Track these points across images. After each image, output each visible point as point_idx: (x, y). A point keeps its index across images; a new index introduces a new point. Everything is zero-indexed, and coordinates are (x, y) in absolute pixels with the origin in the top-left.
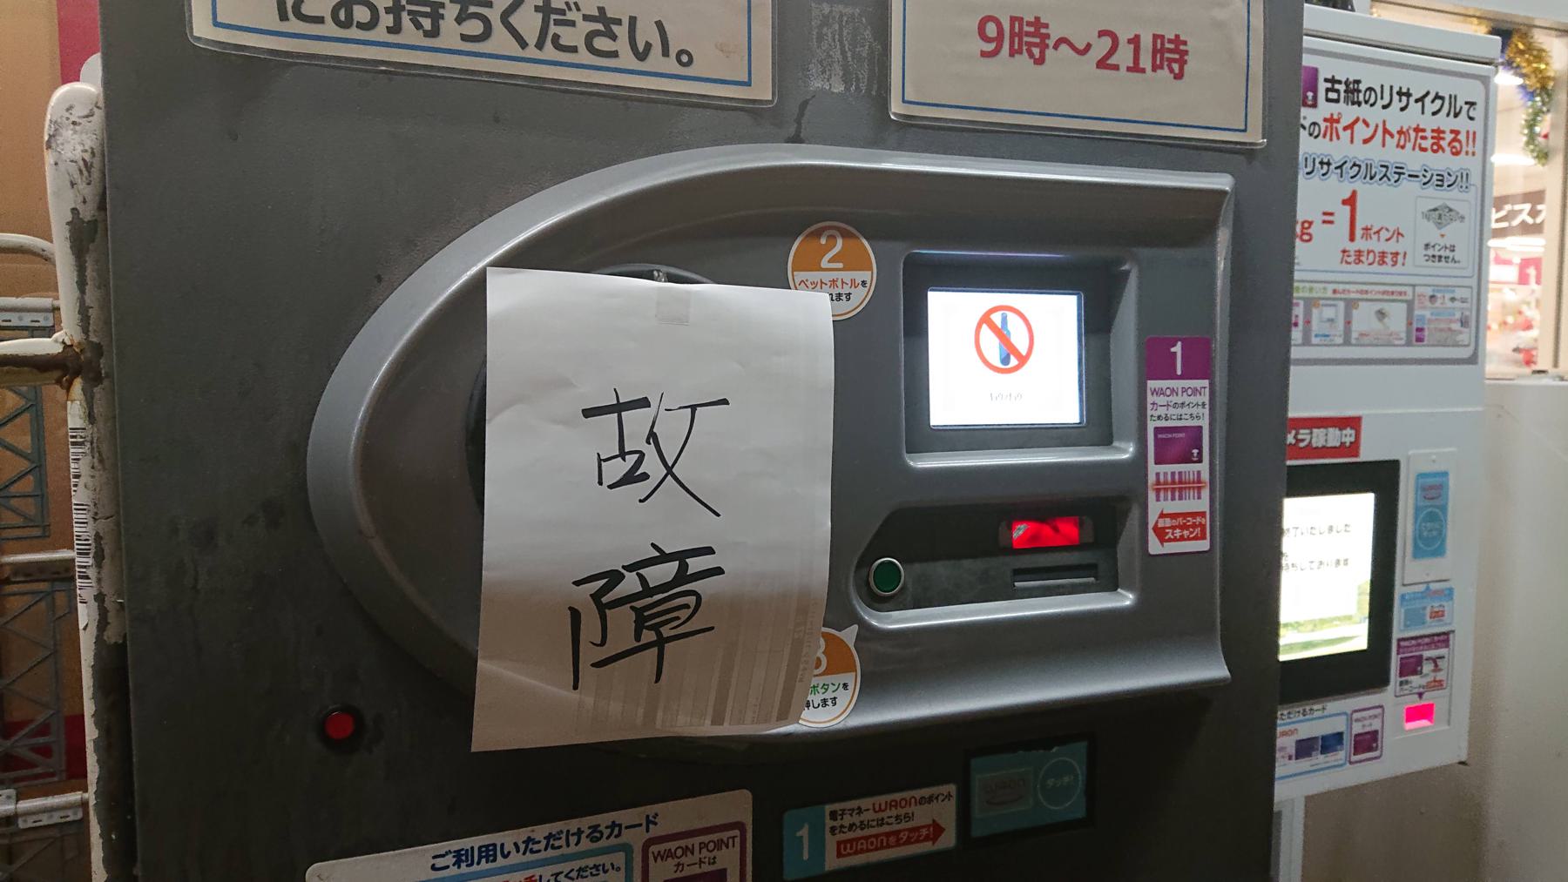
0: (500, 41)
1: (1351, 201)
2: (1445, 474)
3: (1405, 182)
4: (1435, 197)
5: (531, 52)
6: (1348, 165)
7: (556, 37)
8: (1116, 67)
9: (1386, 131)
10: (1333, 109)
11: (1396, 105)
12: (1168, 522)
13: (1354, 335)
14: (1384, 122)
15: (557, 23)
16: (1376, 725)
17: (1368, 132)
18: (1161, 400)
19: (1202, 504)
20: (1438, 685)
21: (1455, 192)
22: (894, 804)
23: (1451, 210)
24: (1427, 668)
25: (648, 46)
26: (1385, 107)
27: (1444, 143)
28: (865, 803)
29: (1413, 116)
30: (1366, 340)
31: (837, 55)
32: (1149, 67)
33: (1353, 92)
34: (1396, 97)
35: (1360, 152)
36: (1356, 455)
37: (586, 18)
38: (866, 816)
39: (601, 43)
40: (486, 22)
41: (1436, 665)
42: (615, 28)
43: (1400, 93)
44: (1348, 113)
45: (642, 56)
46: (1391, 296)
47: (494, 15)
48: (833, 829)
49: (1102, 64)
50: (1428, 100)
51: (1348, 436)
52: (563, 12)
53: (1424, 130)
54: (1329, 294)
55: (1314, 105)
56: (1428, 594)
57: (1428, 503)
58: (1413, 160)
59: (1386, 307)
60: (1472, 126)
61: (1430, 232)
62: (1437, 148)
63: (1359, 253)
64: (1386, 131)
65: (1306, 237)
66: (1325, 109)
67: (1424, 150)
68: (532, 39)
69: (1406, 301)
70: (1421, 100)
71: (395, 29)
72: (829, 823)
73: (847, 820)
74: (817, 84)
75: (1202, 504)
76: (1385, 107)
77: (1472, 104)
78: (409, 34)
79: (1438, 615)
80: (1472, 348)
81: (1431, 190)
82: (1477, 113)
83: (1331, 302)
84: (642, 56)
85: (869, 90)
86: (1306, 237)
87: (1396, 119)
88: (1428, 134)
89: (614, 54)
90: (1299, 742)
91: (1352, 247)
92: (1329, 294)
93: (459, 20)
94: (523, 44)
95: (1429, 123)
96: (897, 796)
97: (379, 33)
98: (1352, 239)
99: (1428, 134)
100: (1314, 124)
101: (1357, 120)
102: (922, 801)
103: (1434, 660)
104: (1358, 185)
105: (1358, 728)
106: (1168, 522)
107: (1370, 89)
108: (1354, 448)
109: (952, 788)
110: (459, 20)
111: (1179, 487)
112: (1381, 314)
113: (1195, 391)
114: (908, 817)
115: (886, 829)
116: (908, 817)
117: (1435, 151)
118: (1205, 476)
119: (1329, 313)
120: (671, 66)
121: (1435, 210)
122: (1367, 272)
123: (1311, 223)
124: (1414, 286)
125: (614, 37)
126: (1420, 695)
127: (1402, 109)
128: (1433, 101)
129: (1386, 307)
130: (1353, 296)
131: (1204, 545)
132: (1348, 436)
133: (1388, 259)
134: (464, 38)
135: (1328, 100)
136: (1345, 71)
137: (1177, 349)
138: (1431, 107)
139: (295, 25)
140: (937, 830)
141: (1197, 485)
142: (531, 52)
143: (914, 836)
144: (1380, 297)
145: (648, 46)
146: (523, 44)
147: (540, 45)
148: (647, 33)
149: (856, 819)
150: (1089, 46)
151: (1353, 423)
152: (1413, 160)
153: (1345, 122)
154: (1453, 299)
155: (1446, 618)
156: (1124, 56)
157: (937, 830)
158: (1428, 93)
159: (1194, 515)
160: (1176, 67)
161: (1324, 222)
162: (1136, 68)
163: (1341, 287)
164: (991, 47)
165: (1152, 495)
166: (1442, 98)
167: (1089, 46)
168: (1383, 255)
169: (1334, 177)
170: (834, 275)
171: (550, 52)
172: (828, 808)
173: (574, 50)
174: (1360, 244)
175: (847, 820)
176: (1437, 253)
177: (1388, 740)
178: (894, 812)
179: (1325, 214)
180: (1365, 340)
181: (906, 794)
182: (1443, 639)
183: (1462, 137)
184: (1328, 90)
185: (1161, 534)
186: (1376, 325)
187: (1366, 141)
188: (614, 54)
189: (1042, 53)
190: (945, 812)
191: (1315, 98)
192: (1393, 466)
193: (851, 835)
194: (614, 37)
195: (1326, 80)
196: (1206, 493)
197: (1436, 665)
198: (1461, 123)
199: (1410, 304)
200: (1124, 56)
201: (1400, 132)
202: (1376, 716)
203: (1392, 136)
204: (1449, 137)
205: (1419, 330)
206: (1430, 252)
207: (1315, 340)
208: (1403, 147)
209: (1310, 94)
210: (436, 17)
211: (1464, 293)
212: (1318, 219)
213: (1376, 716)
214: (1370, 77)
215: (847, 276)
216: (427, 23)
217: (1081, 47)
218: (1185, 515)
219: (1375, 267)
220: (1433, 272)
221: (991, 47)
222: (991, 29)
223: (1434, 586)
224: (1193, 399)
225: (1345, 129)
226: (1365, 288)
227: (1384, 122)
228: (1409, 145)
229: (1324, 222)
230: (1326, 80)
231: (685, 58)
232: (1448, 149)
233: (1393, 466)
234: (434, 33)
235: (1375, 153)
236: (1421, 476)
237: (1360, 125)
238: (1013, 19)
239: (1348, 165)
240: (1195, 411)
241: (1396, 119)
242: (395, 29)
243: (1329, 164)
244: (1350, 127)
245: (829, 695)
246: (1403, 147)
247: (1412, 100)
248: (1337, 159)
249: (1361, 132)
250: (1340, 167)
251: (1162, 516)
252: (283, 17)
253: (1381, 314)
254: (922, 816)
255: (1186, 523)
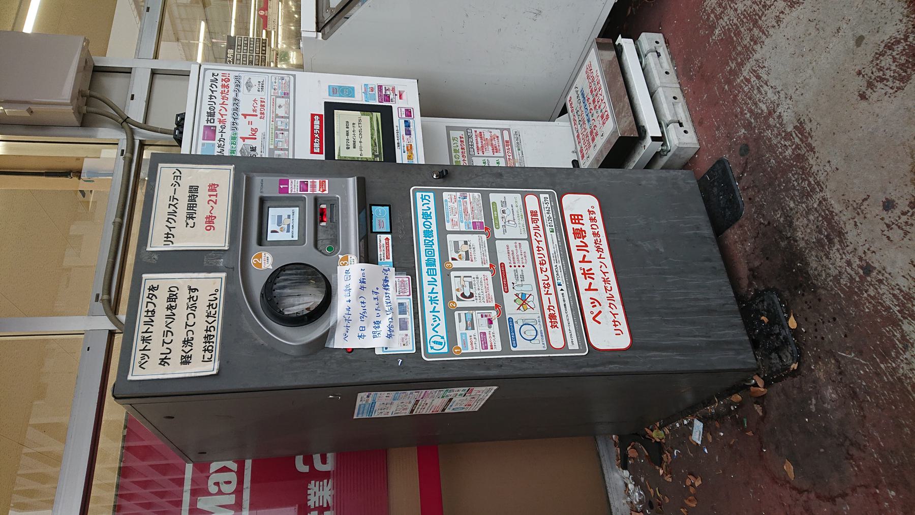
0: (215, 324)
1: (245, 116)
2: (329, 86)
3: (238, 98)
4: (243, 87)
5: (217, 319)
6: (234, 116)
7: (213, 314)
8: (216, 200)
9: (223, 104)
10: (216, 120)
11: (214, 100)
12: (321, 189)
13: (286, 115)
14: (220, 104)
15: (210, 314)
16: (403, 110)
17: (223, 110)
18: (293, 190)
19: (317, 181)
20: (393, 89)
21: (241, 81)
22: (380, 247)
23: (247, 83)
24: (388, 93)
25: (214, 297)
26: (215, 104)
27: (226, 84)
28: (379, 253)
29: (217, 94)
30: (288, 112)
31: (215, 261)
32: (216, 193)
33: (211, 114)
34: (212, 100)
35: (230, 112)
36: (322, 115)
37: (209, 309)
38: (382, 253)
39: (214, 306)
40: (211, 327)
41: (387, 90)
42: (211, 304)
43: (211, 99)
44: (217, 116)
45: (217, 299)
46: (274, 103)
47: (209, 326)
48: (384, 260)
49: (215, 203)
50: (212, 89)
51: (317, 118)
52: (208, 313)
53: (222, 91)
54: (274, 123)
55: (215, 127)
56: (365, 93)
57: (338, 92)
58: (232, 95)
59: (278, 105)
60: (220, 75)
61: (254, 89)
62: (228, 87)
63: (261, 113)
64: (223, 104)
65: (256, 130)
66: (216, 124)
67: (228, 90)
68: (214, 319)
69: (276, 98)
70: (212, 91)
71: (213, 342)
72: (382, 261)
73: (382, 257)
74: (221, 265)
75: (317, 181)
76: (215, 104)
77: (213, 75)
78: (214, 340)
79: (372, 89)
80: (291, 76)
81: (241, 89)
82: (216, 72)
83: (276, 123)
84: (217, 299)
85: (222, 254)
86: (256, 130)
87: (219, 100)
88: (223, 89)
89: (216, 304)
90: (406, 134)
91: (259, 116)
92: (274, 123)
93: (211, 331)
94: (215, 320)
95: (220, 89)
96: (378, 247)
97: (214, 345)
98: (257, 116)
99: (223, 89)
100: (221, 127)
101: (219, 113)
102: (380, 242)
103: (386, 90)
104: (240, 113)
105: (404, 116)
106: (321, 189)
107: (210, 108)
108: (320, 116)
109: (378, 235)
110: (211, 331)
111: (313, 186)
112: (280, 107)
113: (292, 182)
114: (383, 245)
115: (385, 249)
116: (383, 245)
117: (229, 87)
118: (311, 180)
119: (279, 123)
120: (218, 293)
121: (247, 88)
122: (267, 111)
123: (252, 128)
124: (271, 96)
125: (213, 304)
126: (396, 95)
127: (216, 98)
128: (213, 88)
129: (278, 105)
130: (274, 116)
131: (327, 181)
132: (317, 118)
133: (263, 104)
134: (214, 330)
135: (213, 123)
136: (204, 117)
137: (282, 186)
138: (215, 89)
139: (213, 359)
140: (387, 239)
141: (313, 182)
142: (217, 319)
143: (387, 244)
144: (274, 107)
145: (214, 297)
146: (215, 320)
147: (215, 317)
148: (212, 298)
149: (382, 255)
150: (211, 206)
151: (313, 116)
152: (232, 95)
153: (220, 117)
154: (275, 83)
155: (373, 86)
156: (213, 198)
157: (387, 239)
158: (210, 89)
159: (320, 183)
160: (216, 186)
161: (251, 124)
162: (216, 195)
163: (271, 120)
164: (212, 228)
165: (315, 193)
166: (212, 84)
167: (211, 206)
168: (261, 106)
169: (237, 121)
170: (263, 261)
171: (216, 316)
172: (379, 260)
173: (216, 311)
174: (258, 113)
175: (382, 257)
176: (261, 87)
177: (408, 106)
178: (382, 248)
179: (249, 124)
180: (288, 112)
181: (378, 245)
182: (380, 87)
183: (224, 78)
184: (211, 123)
185: (324, 190)
186: (283, 109)
187: (226, 111)
188: (216, 304)
189: (213, 217)
190: (384, 236)
191: (213, 126)
192: (327, 104)
193: (385, 257)
194: (213, 304)
195: (207, 123)
196: (315, 180)
197: (387, 90)
198: (219, 78)
199: (277, 97)
200: (213, 198)
201: (223, 99)
202: (401, 110)
203: (224, 102)
204: (224, 82)
205: (285, 94)
206: (260, 90)
207: (288, 128)
208: (228, 98)
209: (212, 128)
210: (210, 335)
211: (273, 78)
212: (250, 126)
213: (401, 110)
214: (206, 109)
215: (263, 258)
216: (211, 337)
217: (212, 208)
218: (320, 185)
219: (265, 108)
220: (266, 89)
221: (212, 228)
222: (208, 228)
223: (363, 91)
224: (293, 183)
225: (223, 117)
226: (272, 112)
227: (220, 104)
228: (227, 96)
229: (251, 124)
230: (207, 123)
231: (217, 290)
232: (228, 83)
233: (327, 104)
234: (214, 336)
235: (230, 107)
236: (330, 95)
237: (221, 112)
238: (206, 223)
239: (234, 116)
240: (296, 183)
241: (219, 100)
242: (213, 342)
243: (233, 123)
244: (222, 115)
245: (352, 260)
246: (228, 98)
247: (212, 95)
248: (232, 120)
249: (223, 112)
250: (234, 119)
251: (320, 190)
252: (211, 361)
253: (280, 107)
254: (383, 242)
255: (322, 185)
